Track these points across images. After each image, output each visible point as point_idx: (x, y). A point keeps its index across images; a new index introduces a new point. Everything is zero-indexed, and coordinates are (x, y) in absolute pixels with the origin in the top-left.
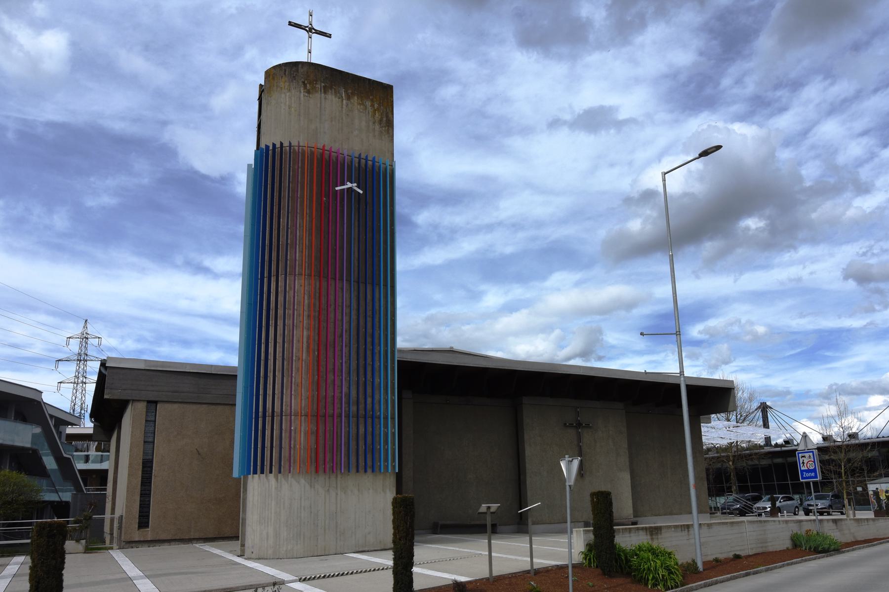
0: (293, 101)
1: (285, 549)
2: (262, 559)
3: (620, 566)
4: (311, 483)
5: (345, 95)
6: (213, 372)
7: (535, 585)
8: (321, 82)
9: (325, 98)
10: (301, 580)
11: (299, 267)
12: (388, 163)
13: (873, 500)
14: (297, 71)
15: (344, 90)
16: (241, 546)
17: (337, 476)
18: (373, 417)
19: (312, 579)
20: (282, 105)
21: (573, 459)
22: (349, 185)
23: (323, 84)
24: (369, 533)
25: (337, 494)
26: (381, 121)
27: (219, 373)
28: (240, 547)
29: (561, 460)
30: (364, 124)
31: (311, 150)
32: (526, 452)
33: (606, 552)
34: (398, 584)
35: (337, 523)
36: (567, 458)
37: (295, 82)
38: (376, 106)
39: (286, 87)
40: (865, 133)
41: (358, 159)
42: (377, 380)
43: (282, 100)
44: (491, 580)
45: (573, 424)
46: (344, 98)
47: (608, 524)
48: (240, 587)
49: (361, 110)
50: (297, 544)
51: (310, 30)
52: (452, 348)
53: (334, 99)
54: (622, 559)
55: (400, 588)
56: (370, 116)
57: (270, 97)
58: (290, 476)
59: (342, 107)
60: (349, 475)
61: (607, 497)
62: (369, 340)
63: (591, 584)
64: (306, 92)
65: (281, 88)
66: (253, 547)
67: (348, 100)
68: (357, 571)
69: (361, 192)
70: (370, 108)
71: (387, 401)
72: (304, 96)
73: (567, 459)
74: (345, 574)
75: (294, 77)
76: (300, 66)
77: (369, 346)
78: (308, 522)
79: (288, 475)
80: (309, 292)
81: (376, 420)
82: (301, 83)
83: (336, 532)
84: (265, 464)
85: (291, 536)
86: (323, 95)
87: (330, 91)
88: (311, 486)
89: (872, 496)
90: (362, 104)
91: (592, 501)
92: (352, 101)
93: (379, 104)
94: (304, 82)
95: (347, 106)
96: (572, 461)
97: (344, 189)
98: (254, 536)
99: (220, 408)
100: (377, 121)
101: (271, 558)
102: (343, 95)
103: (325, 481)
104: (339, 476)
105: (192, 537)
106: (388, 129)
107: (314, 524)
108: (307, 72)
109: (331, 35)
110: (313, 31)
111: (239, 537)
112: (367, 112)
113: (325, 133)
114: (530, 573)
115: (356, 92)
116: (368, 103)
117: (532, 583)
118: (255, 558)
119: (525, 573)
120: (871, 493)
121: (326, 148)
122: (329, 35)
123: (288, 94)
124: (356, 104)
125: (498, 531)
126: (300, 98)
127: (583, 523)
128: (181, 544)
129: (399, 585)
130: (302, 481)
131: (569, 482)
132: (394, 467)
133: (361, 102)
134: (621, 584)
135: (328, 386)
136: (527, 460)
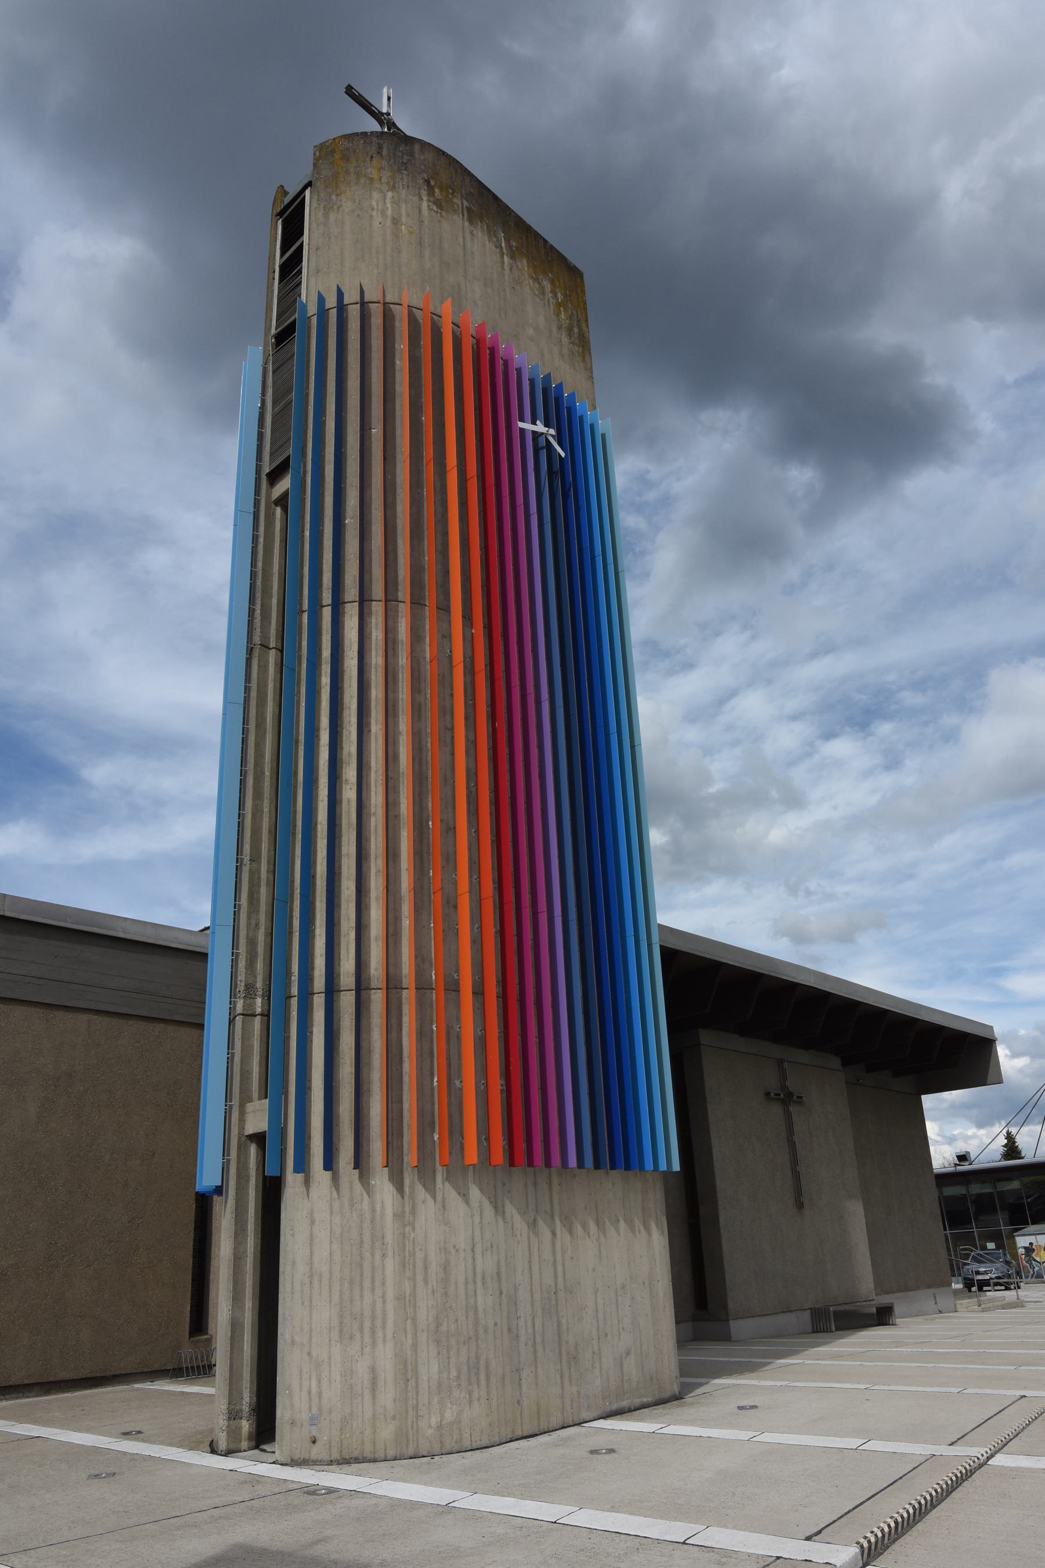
0: (404, 212)
1: (434, 1421)
5: (506, 246)
6: (8, 914)
13: (1024, 1262)
15: (503, 234)
16: (229, 1419)
20: (374, 213)
22: (540, 427)
24: (628, 1353)
25: (554, 1234)
27: (23, 917)
37: (408, 175)
38: (560, 296)
40: (794, 717)
49: (537, 292)
50: (470, 1402)
53: (488, 243)
56: (552, 311)
65: (371, 180)
66: (313, 1421)
70: (550, 295)
76: (417, 147)
78: (496, 1324)
87: (480, 224)
88: (496, 1208)
89: (1023, 1256)
93: (565, 295)
94: (428, 182)
98: (319, 1381)
99: (19, 1011)
100: (564, 326)
101: (391, 1453)
102: (503, 245)
107: (510, 1330)
112: (546, 300)
116: (547, 286)
120: (1021, 1251)
123: (390, 194)
127: (806, 1316)
130: (475, 1193)
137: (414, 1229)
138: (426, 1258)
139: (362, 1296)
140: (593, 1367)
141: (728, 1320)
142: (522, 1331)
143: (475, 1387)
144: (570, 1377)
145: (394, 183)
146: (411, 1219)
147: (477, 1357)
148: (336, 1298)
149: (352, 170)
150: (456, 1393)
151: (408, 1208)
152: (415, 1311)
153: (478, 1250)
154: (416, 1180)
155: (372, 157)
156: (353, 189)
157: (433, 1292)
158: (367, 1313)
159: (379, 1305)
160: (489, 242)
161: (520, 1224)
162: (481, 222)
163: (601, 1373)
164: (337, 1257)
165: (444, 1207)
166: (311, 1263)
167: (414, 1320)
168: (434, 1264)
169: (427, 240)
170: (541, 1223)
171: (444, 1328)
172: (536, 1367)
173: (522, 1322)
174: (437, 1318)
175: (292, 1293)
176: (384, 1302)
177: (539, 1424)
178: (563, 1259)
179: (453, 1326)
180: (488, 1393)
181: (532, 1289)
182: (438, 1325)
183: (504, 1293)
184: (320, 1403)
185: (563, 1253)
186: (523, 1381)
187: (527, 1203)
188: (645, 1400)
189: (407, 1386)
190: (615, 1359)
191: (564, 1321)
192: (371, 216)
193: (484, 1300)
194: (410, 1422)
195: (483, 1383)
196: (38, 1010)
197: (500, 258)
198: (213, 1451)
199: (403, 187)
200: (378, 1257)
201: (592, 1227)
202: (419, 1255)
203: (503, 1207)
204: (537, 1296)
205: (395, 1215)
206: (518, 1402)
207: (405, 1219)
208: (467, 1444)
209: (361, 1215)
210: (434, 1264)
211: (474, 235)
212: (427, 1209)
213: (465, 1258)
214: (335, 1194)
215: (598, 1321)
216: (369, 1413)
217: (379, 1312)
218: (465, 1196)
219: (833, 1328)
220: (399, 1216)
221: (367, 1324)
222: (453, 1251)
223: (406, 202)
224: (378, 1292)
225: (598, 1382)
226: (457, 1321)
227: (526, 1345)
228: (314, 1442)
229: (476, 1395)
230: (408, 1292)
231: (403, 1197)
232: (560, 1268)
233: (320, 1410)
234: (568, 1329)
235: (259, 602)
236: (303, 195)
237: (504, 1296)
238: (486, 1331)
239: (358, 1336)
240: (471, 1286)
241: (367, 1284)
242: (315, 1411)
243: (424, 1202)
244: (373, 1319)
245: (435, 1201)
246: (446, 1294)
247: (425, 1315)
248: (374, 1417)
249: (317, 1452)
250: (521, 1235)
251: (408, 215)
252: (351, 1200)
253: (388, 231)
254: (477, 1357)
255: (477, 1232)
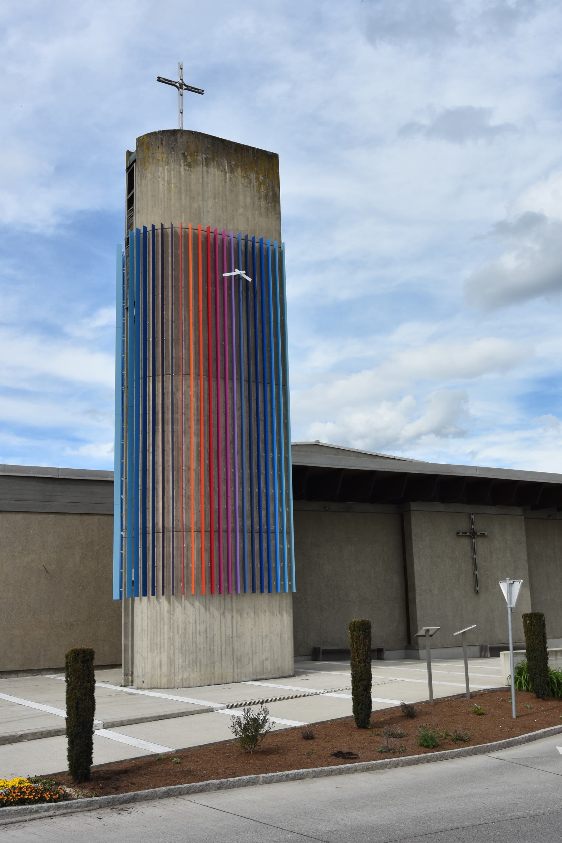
0: (172, 176)
1: (180, 677)
2: (155, 688)
3: (552, 690)
4: (206, 605)
5: (228, 168)
6: (60, 477)
7: (479, 707)
8: (202, 153)
9: (207, 172)
10: (229, 707)
11: (185, 365)
12: (276, 244)
14: (176, 140)
15: (226, 161)
16: (125, 676)
17: (232, 597)
18: (267, 532)
19: (238, 706)
21: (514, 582)
22: (237, 272)
23: (204, 156)
24: (267, 659)
25: (232, 617)
26: (267, 195)
27: (66, 477)
28: (123, 677)
29: (501, 582)
30: (249, 199)
31: (194, 232)
32: (415, 566)
33: (540, 675)
34: (358, 705)
35: (233, 649)
36: (508, 580)
37: (175, 154)
38: (261, 178)
39: (164, 159)
41: (244, 241)
42: (271, 491)
43: (160, 174)
44: (432, 703)
45: (466, 533)
46: (227, 171)
47: (542, 646)
48: (173, 714)
49: (246, 184)
50: (193, 672)
51: (181, 86)
52: (318, 441)
53: (217, 172)
54: (554, 681)
55: (361, 709)
56: (255, 191)
57: (145, 170)
58: (183, 599)
59: (226, 182)
60: (244, 596)
61: (540, 619)
62: (262, 446)
63: (529, 706)
64: (187, 166)
65: (158, 160)
66: (143, 676)
67: (231, 173)
68: (280, 698)
69: (250, 280)
70: (255, 181)
71: (281, 514)
72: (185, 170)
73: (508, 582)
74: (269, 701)
75: (172, 147)
76: (179, 135)
77: (262, 454)
78: (204, 648)
79: (181, 597)
80: (198, 394)
81: (272, 536)
82: (180, 155)
83: (233, 658)
84: (139, 586)
85: (187, 663)
86: (205, 168)
87: (212, 163)
88: (206, 608)
90: (247, 177)
91: (525, 621)
92: (235, 174)
93: (264, 177)
94: (184, 154)
95: (230, 180)
96: (513, 583)
97: (231, 276)
98: (145, 664)
99: (69, 517)
101: (166, 687)
102: (226, 168)
103: (220, 606)
104: (234, 598)
105: (42, 668)
106: (275, 205)
107: (210, 650)
108: (187, 142)
109: (203, 91)
110: (184, 87)
111: (121, 664)
113: (208, 212)
114: (465, 697)
115: (240, 164)
116: (253, 176)
117: (476, 705)
118: (147, 687)
119: (459, 696)
121: (212, 230)
122: (201, 91)
123: (166, 167)
124: (240, 177)
125: (385, 657)
126: (180, 172)
128: (29, 676)
129: (360, 706)
130: (197, 604)
131: (510, 605)
132: (291, 587)
133: (245, 175)
134: (557, 707)
135: (220, 498)
136: (416, 576)
137: (174, 616)
138: (178, 626)
139: (157, 638)
140: (249, 663)
141: (418, 650)
142: (216, 650)
143: (195, 668)
144: (237, 666)
145: (168, 160)
146: (173, 612)
147: (196, 658)
148: (149, 638)
149: (150, 155)
150: (188, 669)
151: (172, 609)
152: (174, 643)
153: (198, 623)
154: (175, 599)
155: (159, 147)
156: (151, 166)
157: (180, 637)
158: (159, 643)
159: (162, 641)
160: (218, 171)
161: (217, 614)
162: (213, 162)
163: (252, 665)
164: (150, 625)
165: (185, 609)
166: (142, 627)
167: (174, 645)
168: (181, 627)
169: (183, 189)
170: (227, 613)
171: (184, 648)
172: (222, 662)
173: (216, 647)
174: (182, 645)
175: (137, 636)
176: (164, 640)
177: (222, 681)
178: (237, 626)
179: (187, 648)
180: (200, 670)
181: (221, 636)
182: (182, 648)
183: (208, 637)
184: (145, 671)
185: (237, 623)
186: (216, 667)
187: (220, 606)
188: (274, 676)
189: (171, 666)
190: (260, 661)
191: (236, 647)
192: (159, 181)
193: (200, 640)
194: (172, 677)
195: (198, 666)
196: (76, 516)
197: (224, 177)
198: (121, 686)
199: (172, 161)
200: (162, 626)
201: (252, 614)
202: (176, 625)
203: (209, 608)
204: (223, 638)
205: (168, 611)
206: (213, 673)
207: (171, 612)
208: (192, 685)
209: (157, 611)
210: (181, 627)
211: (208, 172)
212: (179, 609)
213: (192, 626)
214: (149, 604)
215: (252, 648)
216: (159, 674)
217: (162, 643)
218: (193, 605)
219: (489, 656)
220: (169, 612)
221: (159, 647)
222: (188, 623)
223: (174, 170)
224: (162, 636)
225: (251, 669)
226: (189, 646)
227: (217, 655)
228: (143, 682)
229: (195, 670)
230: (172, 636)
231: (170, 605)
232: (235, 629)
233: (145, 673)
234: (237, 650)
235: (125, 368)
236: (132, 167)
237: (208, 638)
238: (200, 650)
239: (156, 650)
240: (194, 635)
241: (159, 633)
242: (143, 673)
243: (177, 607)
244: (160, 645)
245: (182, 606)
246: (185, 637)
247: (177, 643)
248: (161, 675)
249: (144, 685)
250: (217, 618)
251: (174, 177)
252: (154, 606)
253: (166, 189)
254: (196, 658)
255: (198, 617)
